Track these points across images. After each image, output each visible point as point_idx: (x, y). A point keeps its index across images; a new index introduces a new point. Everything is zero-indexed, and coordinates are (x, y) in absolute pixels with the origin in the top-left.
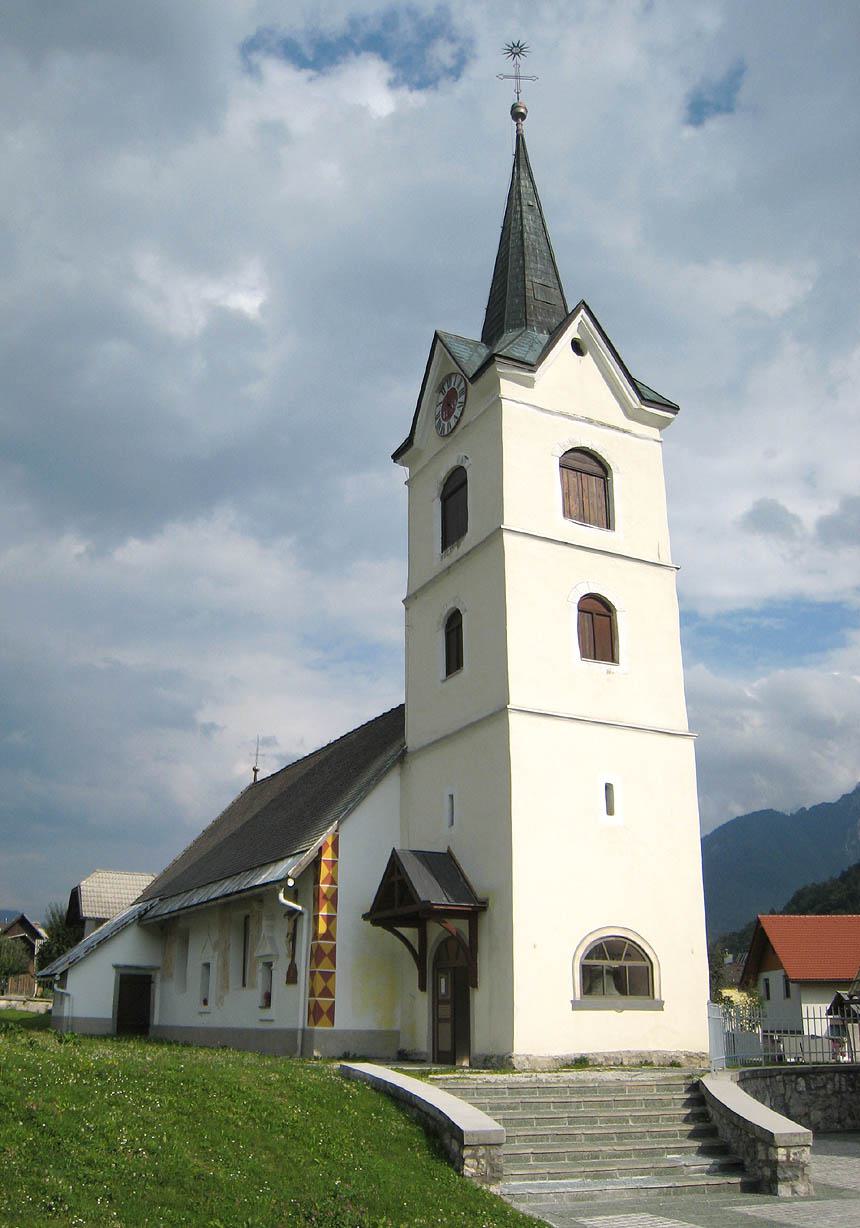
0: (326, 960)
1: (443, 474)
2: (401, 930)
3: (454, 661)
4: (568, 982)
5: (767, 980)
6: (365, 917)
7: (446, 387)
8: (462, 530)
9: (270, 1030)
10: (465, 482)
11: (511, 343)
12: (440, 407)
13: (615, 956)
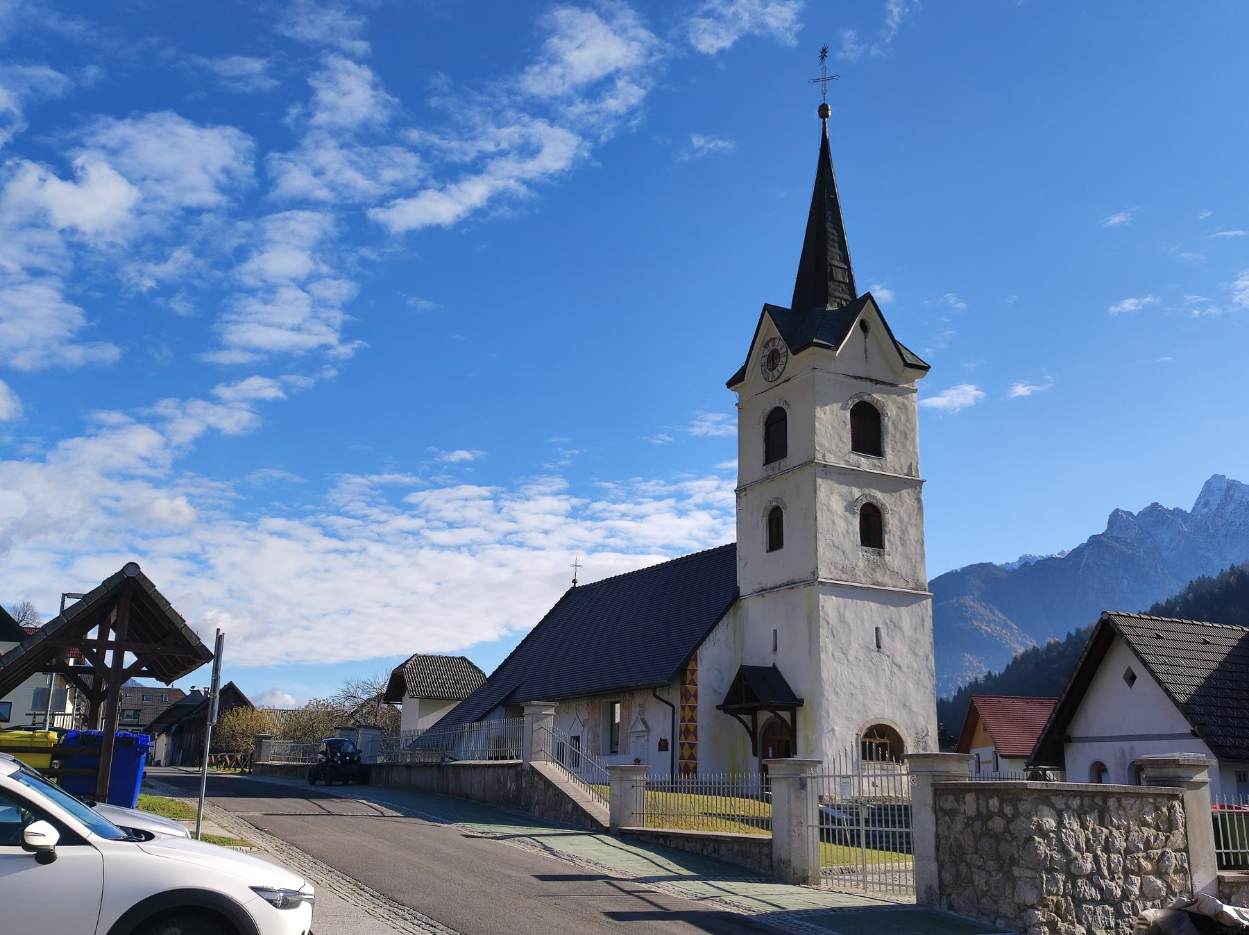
5: (978, 755)
6: (719, 708)
7: (770, 344)
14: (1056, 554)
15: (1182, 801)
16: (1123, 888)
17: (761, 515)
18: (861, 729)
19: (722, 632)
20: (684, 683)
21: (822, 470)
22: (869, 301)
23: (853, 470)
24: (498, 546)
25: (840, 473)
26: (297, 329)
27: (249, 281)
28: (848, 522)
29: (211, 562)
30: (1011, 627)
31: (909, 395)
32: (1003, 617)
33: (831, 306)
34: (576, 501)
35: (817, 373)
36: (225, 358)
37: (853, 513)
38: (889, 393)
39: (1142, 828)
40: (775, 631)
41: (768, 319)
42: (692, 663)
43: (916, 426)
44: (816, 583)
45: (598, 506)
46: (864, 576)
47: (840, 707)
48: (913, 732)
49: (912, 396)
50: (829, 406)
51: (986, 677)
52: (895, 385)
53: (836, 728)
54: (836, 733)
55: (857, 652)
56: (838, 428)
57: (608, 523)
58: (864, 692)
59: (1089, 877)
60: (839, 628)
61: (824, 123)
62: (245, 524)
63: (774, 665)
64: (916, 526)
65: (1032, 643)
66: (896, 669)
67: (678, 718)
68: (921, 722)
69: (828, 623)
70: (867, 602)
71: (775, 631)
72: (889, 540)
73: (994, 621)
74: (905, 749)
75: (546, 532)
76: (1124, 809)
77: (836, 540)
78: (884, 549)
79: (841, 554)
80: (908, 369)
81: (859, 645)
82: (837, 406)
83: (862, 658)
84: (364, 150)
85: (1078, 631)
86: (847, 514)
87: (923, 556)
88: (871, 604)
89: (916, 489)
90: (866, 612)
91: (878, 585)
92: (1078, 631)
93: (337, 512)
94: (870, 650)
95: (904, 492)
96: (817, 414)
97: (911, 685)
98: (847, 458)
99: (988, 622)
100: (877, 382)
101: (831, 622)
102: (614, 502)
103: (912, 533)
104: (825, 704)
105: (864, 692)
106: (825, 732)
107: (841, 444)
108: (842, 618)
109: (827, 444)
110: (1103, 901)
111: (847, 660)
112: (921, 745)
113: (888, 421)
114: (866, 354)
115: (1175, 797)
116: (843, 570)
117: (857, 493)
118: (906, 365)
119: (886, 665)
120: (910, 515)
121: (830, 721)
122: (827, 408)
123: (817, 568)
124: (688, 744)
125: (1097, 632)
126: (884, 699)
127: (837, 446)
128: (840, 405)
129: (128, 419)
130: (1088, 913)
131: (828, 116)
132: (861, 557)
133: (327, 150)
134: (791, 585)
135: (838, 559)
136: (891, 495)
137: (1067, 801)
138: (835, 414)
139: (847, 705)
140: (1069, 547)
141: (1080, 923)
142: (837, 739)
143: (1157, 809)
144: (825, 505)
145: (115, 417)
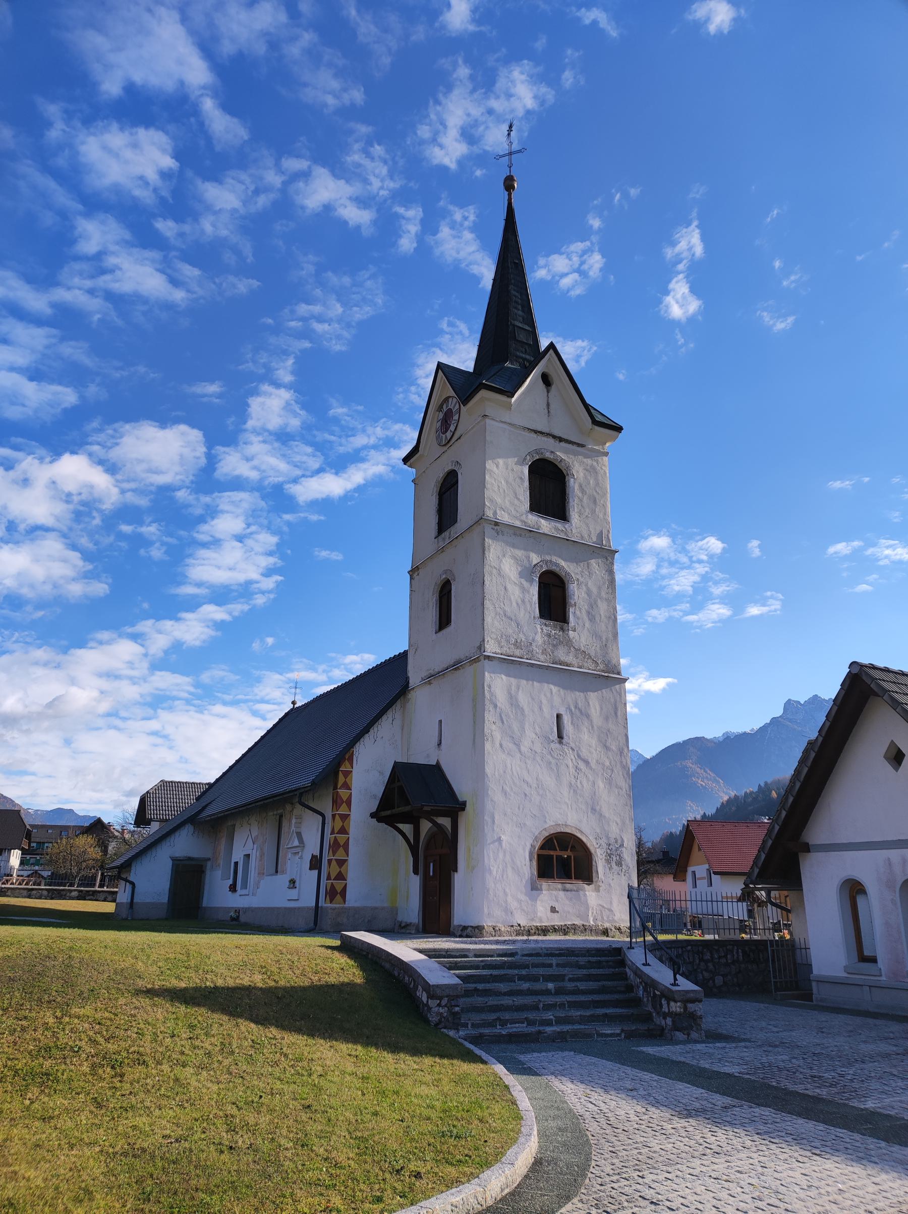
0: (341, 850)
1: (441, 475)
2: (401, 826)
3: (444, 620)
4: (527, 867)
6: (373, 815)
8: (454, 521)
9: (299, 908)
10: (457, 482)
11: (494, 375)
12: (440, 423)
13: (564, 848)
14: (748, 731)
17: (431, 594)
19: (386, 728)
20: (335, 788)
22: (551, 352)
23: (531, 531)
28: (523, 590)
30: (719, 782)
31: (600, 459)
32: (713, 775)
35: (488, 421)
36: (189, 590)
37: (531, 581)
38: (576, 454)
40: (440, 721)
41: (442, 377)
44: (482, 658)
46: (543, 653)
47: (509, 810)
48: (603, 842)
49: (602, 459)
51: (702, 816)
52: (582, 446)
55: (533, 742)
56: (513, 483)
58: (541, 793)
61: (510, 195)
63: (438, 762)
64: (607, 600)
65: (732, 794)
66: (582, 765)
67: (328, 830)
68: (614, 830)
69: (496, 706)
70: (546, 685)
71: (440, 721)
73: (707, 777)
74: (594, 863)
79: (513, 624)
80: (596, 428)
81: (536, 734)
82: (512, 461)
83: (539, 751)
85: (766, 783)
86: (523, 581)
87: (615, 635)
88: (552, 687)
89: (607, 560)
90: (545, 695)
91: (560, 664)
92: (766, 783)
93: (263, 701)
96: (487, 466)
97: (601, 784)
98: (523, 518)
99: (703, 778)
100: (561, 440)
103: (603, 607)
104: (489, 806)
106: (489, 842)
107: (516, 502)
108: (513, 700)
109: (499, 501)
112: (614, 858)
114: (548, 408)
116: (517, 645)
119: (570, 759)
120: (599, 588)
121: (495, 828)
123: (484, 640)
125: (836, 708)
126: (567, 800)
127: (512, 504)
128: (516, 459)
129: (114, 636)
131: (513, 188)
132: (539, 630)
134: (456, 666)
135: (510, 631)
138: (509, 468)
139: (519, 808)
140: (757, 725)
142: (505, 852)
145: (105, 635)
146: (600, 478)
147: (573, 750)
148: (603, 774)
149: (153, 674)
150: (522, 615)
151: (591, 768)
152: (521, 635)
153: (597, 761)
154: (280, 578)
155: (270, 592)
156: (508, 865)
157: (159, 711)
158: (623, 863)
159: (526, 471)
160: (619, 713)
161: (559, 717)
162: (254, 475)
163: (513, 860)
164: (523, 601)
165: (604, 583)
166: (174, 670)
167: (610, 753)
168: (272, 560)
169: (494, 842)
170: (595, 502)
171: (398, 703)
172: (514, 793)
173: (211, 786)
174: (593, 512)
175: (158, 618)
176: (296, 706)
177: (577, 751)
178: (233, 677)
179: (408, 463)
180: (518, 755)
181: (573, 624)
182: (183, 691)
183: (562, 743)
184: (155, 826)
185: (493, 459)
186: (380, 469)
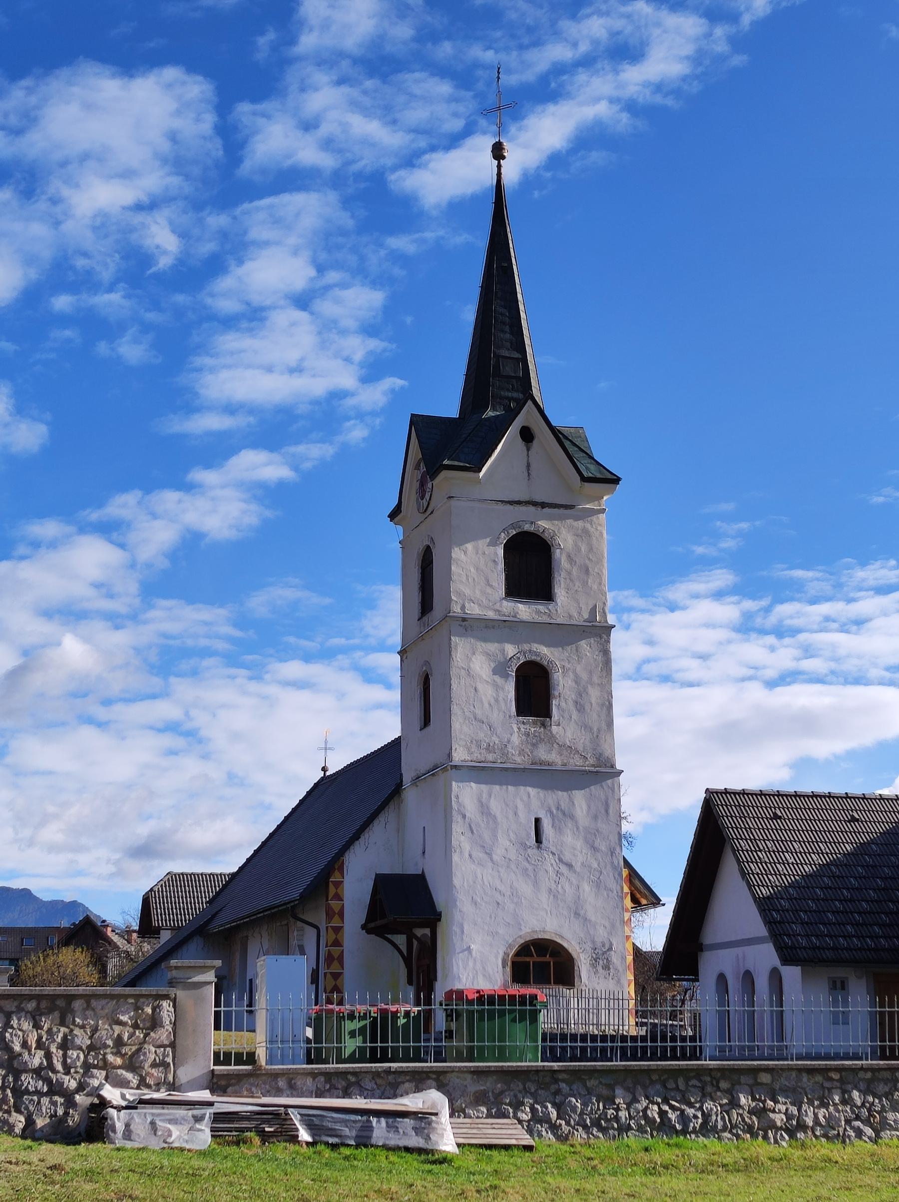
0: (336, 964)
3: (426, 721)
15: (174, 1001)
16: (80, 1081)
18: (510, 946)
19: (378, 833)
20: (327, 900)
21: (461, 626)
23: (505, 621)
24: (629, 683)
25: (486, 627)
26: (296, 370)
27: (227, 306)
28: (496, 687)
29: (203, 733)
31: (594, 518)
33: (494, 409)
34: (749, 605)
35: (453, 502)
36: (212, 422)
37: (506, 676)
38: (562, 518)
39: (114, 1026)
42: (337, 873)
43: (603, 557)
45: (785, 610)
46: (520, 754)
47: (479, 920)
48: (588, 946)
50: (473, 543)
52: (571, 507)
53: (472, 946)
54: (474, 953)
55: (506, 850)
57: (802, 637)
58: (515, 900)
59: (37, 1072)
60: (481, 822)
61: (499, 166)
62: (243, 672)
66: (564, 869)
69: (464, 816)
70: (522, 788)
72: (559, 706)
75: (703, 657)
76: (93, 1010)
77: (479, 712)
78: (550, 718)
80: (586, 484)
82: (483, 543)
83: (513, 857)
84: (369, 84)
86: (497, 678)
88: (530, 789)
89: (601, 638)
90: (522, 800)
94: (525, 847)
95: (583, 643)
96: (453, 555)
97: (586, 887)
98: (497, 607)
100: (543, 505)
101: (467, 815)
102: (814, 601)
103: (594, 694)
104: (457, 917)
105: (515, 900)
107: (489, 590)
108: (484, 809)
109: (467, 591)
110: (51, 1092)
111: (492, 860)
112: (601, 962)
113: (561, 554)
114: (528, 470)
115: (166, 997)
116: (489, 749)
117: (511, 650)
118: (584, 479)
120: (591, 673)
121: (464, 938)
122: (469, 546)
124: (331, 973)
126: (546, 906)
127: (483, 593)
128: (488, 540)
129: (71, 529)
130: (30, 1102)
132: (516, 730)
133: (316, 89)
135: (481, 735)
136: (563, 649)
137: (21, 1003)
139: (491, 917)
141: (18, 1111)
142: (475, 960)
143: (137, 1008)
144: (463, 668)
145: (49, 529)
146: (594, 542)
147: (553, 854)
148: (589, 877)
149: (151, 607)
150: (495, 715)
151: (575, 872)
152: (494, 738)
153: (582, 864)
154: (399, 382)
155: (374, 414)
156: (479, 973)
157: (173, 680)
158: (611, 966)
159: (501, 552)
160: (611, 811)
161: (537, 821)
162: (327, 161)
163: (484, 968)
164: (497, 700)
165: (597, 667)
166: (191, 598)
167: (599, 855)
168: (374, 344)
169: (463, 951)
170: (587, 571)
171: (392, 805)
172: (486, 902)
173: (233, 876)
174: (585, 583)
175: (149, 486)
176: (328, 773)
177: (558, 855)
178: (316, 600)
179: (396, 519)
180: (490, 864)
181: (556, 718)
182: (218, 637)
183: (541, 848)
184: (166, 936)
185: (460, 545)
186: (602, 109)
